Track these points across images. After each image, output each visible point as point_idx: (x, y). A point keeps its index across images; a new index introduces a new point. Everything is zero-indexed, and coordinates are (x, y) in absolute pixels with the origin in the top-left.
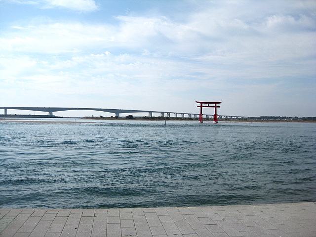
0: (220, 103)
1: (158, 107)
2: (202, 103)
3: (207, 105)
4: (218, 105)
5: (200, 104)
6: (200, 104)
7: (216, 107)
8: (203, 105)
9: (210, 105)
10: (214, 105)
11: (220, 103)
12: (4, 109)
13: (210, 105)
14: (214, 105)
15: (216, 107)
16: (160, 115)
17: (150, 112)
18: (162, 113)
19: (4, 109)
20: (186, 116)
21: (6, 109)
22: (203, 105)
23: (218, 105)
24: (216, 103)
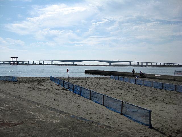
2: (12, 58)
5: (11, 58)
6: (11, 58)
7: (16, 59)
8: (13, 58)
12: (51, 61)
16: (136, 64)
19: (51, 61)
23: (17, 58)
24: (16, 58)
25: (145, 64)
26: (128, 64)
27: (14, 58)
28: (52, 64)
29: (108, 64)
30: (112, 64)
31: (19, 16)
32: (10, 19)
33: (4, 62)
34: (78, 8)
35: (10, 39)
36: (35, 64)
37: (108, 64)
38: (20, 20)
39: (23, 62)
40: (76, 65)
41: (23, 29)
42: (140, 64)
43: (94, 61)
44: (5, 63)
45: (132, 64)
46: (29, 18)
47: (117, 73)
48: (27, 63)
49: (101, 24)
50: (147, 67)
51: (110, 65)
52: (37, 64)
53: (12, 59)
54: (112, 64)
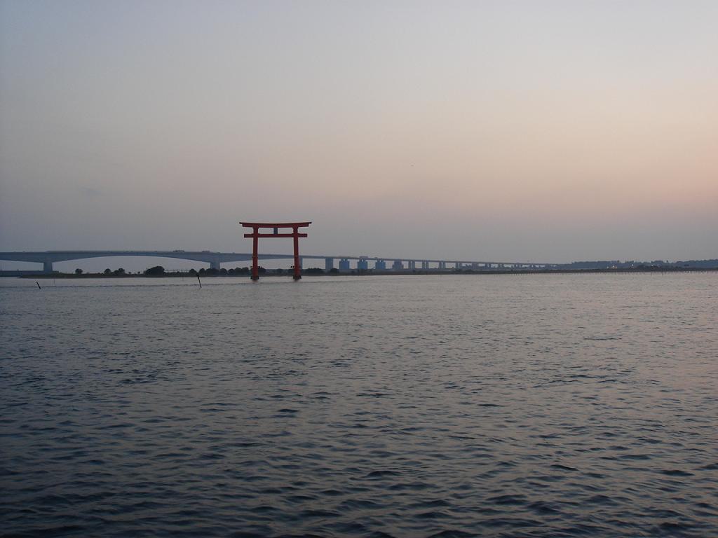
0: (306, 224)
2: (256, 226)
4: (301, 230)
5: (250, 230)
6: (250, 230)
7: (296, 236)
8: (261, 231)
9: (281, 231)
10: (290, 231)
11: (306, 224)
12: (251, 252)
13: (281, 231)
14: (290, 231)
15: (296, 236)
19: (421, 263)
22: (261, 231)
23: (301, 230)
24: (295, 226)
53: (256, 236)
54: (39, 267)
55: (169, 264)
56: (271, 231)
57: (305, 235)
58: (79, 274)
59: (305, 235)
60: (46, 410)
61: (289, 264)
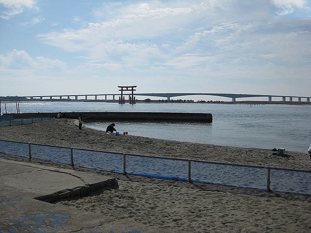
0: (135, 87)
1: (278, 90)
2: (122, 87)
3: (126, 89)
4: (134, 88)
5: (121, 89)
6: (121, 89)
7: (132, 90)
8: (124, 89)
9: (129, 89)
10: (131, 89)
11: (135, 87)
12: (105, 96)
13: (129, 89)
14: (131, 89)
15: (132, 90)
16: (281, 99)
17: (270, 97)
18: (284, 97)
19: (105, 96)
20: (295, 100)
21: (86, 96)
22: (124, 89)
23: (134, 88)
24: (132, 87)
25: (296, 100)
26: (267, 99)
27: (127, 87)
28: (96, 101)
29: (230, 100)
30: (237, 100)
31: (76, 19)
32: (55, 24)
33: (41, 97)
34: (178, 11)
35: (43, 57)
36: (99, 101)
37: (230, 100)
38: (76, 27)
39: (76, 96)
40: (173, 101)
41: (77, 42)
42: (288, 99)
43: (201, 94)
44: (43, 98)
45: (273, 99)
46: (91, 24)
47: (94, 115)
48: (84, 98)
49: (210, 33)
50: (70, 103)
51: (234, 102)
52: (74, 100)
53: (122, 90)
54: (237, 100)
55: (152, 98)
56: (126, 89)
57: (135, 90)
58: (192, 102)
59: (135, 90)
60: (279, 164)
61: (117, 98)
